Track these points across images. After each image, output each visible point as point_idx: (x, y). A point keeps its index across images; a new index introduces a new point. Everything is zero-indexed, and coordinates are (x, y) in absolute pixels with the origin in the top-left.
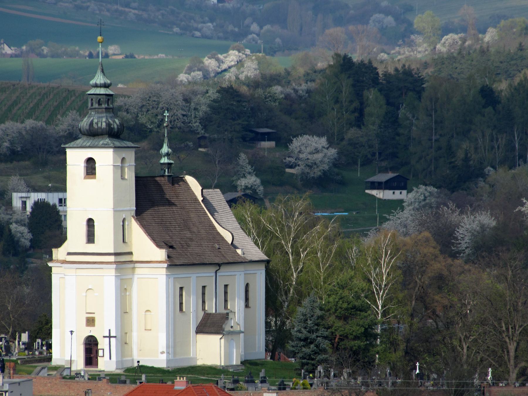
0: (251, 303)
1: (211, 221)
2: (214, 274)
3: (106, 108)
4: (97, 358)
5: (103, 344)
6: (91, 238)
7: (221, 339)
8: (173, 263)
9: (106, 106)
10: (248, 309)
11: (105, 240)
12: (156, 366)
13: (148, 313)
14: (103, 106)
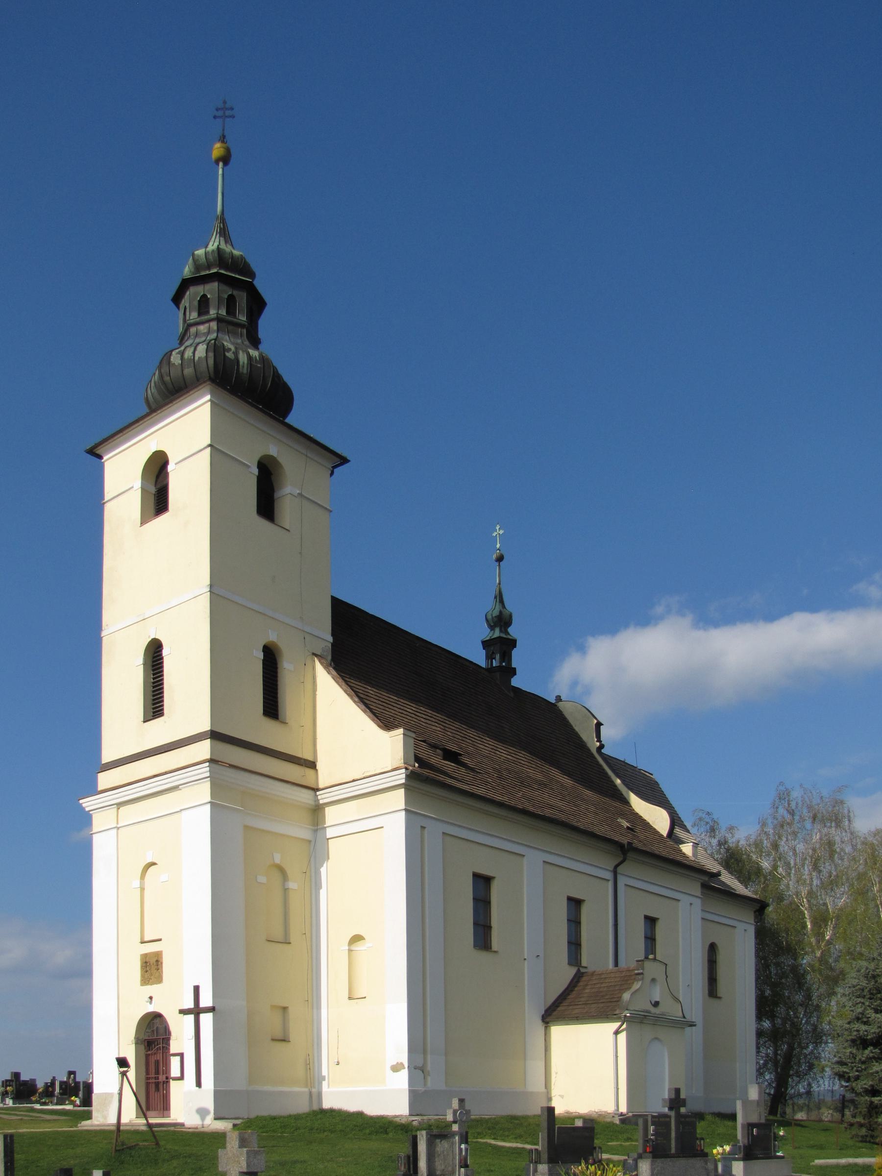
0: (722, 989)
1: (604, 770)
2: (609, 875)
3: (219, 320)
4: (168, 1082)
5: (181, 1037)
6: (155, 705)
7: (617, 1033)
8: (426, 777)
9: (223, 312)
10: (714, 1001)
11: (191, 701)
12: (373, 1109)
13: (358, 947)
14: (213, 312)
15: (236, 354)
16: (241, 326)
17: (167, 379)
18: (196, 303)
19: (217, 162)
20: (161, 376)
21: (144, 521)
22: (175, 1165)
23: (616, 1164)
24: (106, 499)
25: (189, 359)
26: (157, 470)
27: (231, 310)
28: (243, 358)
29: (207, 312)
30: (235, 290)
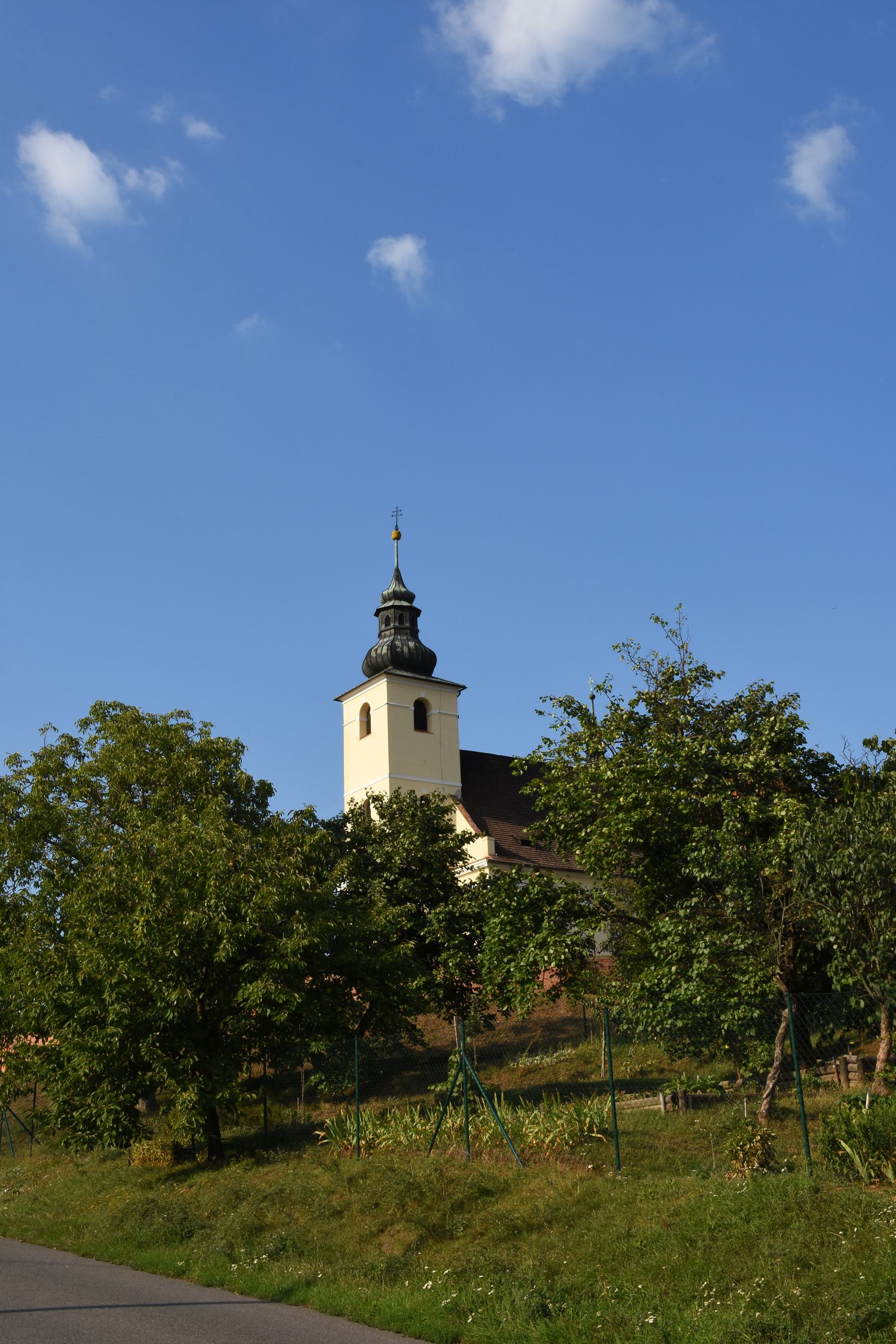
3: (395, 628)
9: (397, 624)
14: (392, 625)
15: (402, 648)
16: (407, 628)
21: (361, 738)
23: (771, 1052)
26: (366, 710)
28: (406, 649)
30: (402, 613)
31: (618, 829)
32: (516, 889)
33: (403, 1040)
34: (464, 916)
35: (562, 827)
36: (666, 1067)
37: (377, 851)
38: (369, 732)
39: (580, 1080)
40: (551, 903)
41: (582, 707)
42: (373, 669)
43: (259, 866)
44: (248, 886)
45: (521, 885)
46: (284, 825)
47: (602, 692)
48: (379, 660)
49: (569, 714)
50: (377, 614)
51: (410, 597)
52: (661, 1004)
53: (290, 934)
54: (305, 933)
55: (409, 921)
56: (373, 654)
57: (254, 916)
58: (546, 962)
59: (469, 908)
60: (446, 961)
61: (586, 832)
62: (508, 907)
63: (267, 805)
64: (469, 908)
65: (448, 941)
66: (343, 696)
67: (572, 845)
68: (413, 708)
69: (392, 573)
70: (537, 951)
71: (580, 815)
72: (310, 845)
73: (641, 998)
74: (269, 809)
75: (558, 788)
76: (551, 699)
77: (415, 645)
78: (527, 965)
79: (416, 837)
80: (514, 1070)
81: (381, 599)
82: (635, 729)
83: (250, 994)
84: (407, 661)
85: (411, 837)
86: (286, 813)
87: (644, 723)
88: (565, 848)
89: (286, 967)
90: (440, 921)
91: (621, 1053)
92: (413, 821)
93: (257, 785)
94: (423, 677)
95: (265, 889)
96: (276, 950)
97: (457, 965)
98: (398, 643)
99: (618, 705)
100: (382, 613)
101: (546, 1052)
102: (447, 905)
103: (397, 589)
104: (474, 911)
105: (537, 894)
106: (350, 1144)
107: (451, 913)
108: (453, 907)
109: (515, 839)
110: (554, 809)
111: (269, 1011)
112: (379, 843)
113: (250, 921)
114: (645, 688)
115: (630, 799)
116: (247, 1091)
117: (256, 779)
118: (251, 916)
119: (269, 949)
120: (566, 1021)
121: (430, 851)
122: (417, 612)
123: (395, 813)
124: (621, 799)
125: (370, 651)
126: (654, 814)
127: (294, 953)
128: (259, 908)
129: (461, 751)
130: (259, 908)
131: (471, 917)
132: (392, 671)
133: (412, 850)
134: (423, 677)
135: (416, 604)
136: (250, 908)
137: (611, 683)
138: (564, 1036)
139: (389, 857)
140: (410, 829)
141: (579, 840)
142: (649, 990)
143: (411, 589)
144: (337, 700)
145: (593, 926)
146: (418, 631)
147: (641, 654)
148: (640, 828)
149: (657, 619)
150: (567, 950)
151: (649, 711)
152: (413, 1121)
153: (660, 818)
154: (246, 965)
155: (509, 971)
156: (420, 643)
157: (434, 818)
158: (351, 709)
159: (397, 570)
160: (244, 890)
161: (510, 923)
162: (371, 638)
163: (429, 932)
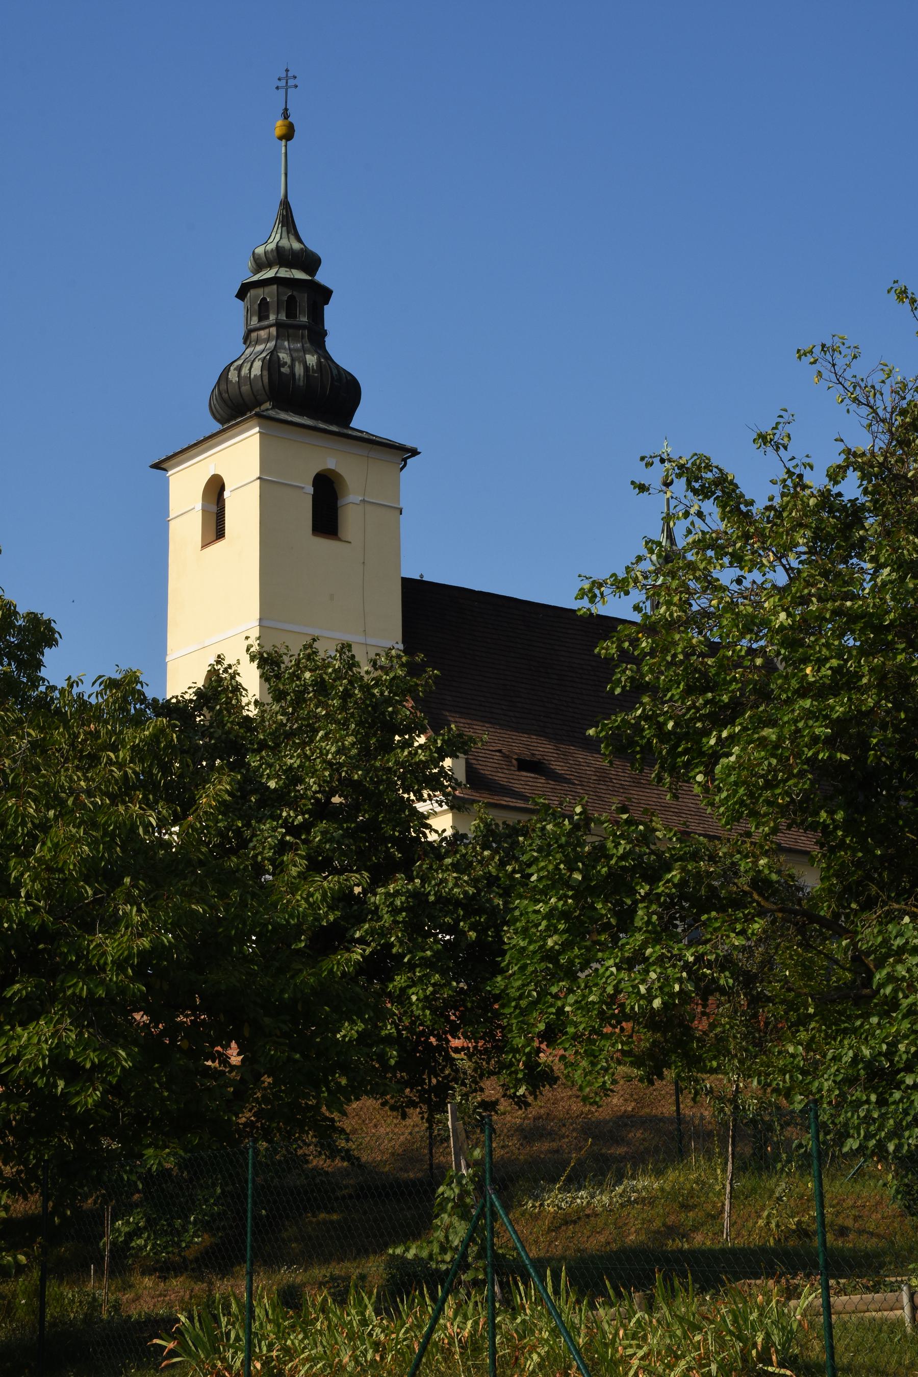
3: (278, 325)
9: (283, 317)
14: (272, 317)
15: (292, 367)
17: (225, 396)
18: (256, 307)
19: (280, 138)
20: (220, 393)
21: (205, 546)
22: (903, 1049)
24: (171, 517)
25: (245, 377)
26: (215, 490)
27: (291, 314)
28: (299, 370)
29: (267, 317)
30: (293, 295)
31: (798, 731)
32: (582, 845)
33: (305, 1150)
34: (446, 902)
35: (670, 725)
36: (849, 1223)
37: (270, 766)
38: (220, 533)
39: (672, 1245)
40: (652, 878)
41: (725, 480)
42: (233, 408)
43: (46, 784)
44: (23, 824)
45: (589, 839)
46: (83, 704)
47: (770, 449)
48: (245, 389)
49: (695, 492)
50: (242, 294)
51: (310, 262)
52: (897, 1095)
53: (112, 924)
54: (144, 924)
55: (331, 908)
56: (233, 376)
57: (37, 886)
58: (642, 997)
59: (456, 885)
60: (403, 990)
61: (719, 738)
62: (567, 883)
63: (39, 664)
64: (456, 885)
65: (410, 952)
66: (169, 458)
67: (687, 765)
68: (310, 490)
69: (274, 210)
70: (624, 975)
71: (707, 702)
72: (133, 748)
73: (851, 1081)
74: (43, 673)
75: (675, 644)
76: (662, 461)
77: (319, 363)
78: (602, 1002)
79: (351, 739)
80: (535, 1218)
81: (250, 263)
82: (834, 529)
83: (25, 1047)
84: (300, 393)
85: (342, 739)
86: (88, 680)
87: (853, 515)
88: (673, 770)
89: (101, 992)
90: (395, 911)
91: (754, 1190)
92: (343, 708)
93: (20, 622)
94: (334, 428)
95: (60, 832)
96: (79, 958)
97: (427, 1001)
98: (284, 356)
99: (800, 476)
100: (252, 293)
101: (600, 1184)
102: (411, 879)
103: (285, 243)
104: (465, 893)
105: (623, 858)
106: (229, 1368)
107: (418, 896)
108: (423, 882)
109: (505, 756)
110: (653, 689)
111: (61, 1084)
112: (272, 749)
113: (28, 896)
114: (863, 442)
115: (826, 671)
116: (7, 1250)
117: (22, 610)
118: (29, 885)
119: (65, 955)
120: (625, 1121)
121: (377, 769)
122: (325, 294)
123: (306, 691)
124: (808, 671)
125: (227, 370)
126: (877, 703)
127: (120, 965)
128: (49, 869)
129: (404, 580)
130: (49, 869)
131: (458, 903)
132: (272, 413)
133: (341, 765)
134: (334, 428)
135: (321, 277)
136: (28, 868)
137: (788, 429)
138: (621, 1150)
139: (293, 777)
140: (337, 722)
141: (702, 754)
142: (869, 1065)
143: (312, 246)
144: (157, 466)
145: (739, 927)
146: (325, 333)
147: (861, 369)
148: (847, 732)
149: (903, 294)
150: (684, 974)
151: (866, 492)
152: (364, 1322)
153: (888, 712)
154: (17, 987)
155: (560, 1011)
156: (328, 358)
157: (388, 701)
158: (186, 486)
159: (285, 205)
160: (15, 832)
161: (565, 915)
162: (228, 342)
163: (372, 932)
